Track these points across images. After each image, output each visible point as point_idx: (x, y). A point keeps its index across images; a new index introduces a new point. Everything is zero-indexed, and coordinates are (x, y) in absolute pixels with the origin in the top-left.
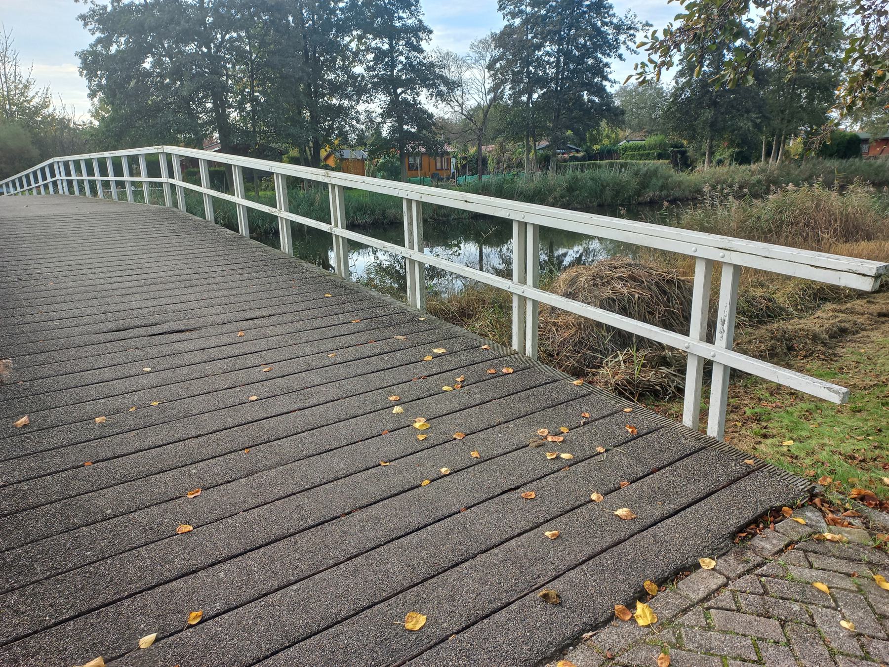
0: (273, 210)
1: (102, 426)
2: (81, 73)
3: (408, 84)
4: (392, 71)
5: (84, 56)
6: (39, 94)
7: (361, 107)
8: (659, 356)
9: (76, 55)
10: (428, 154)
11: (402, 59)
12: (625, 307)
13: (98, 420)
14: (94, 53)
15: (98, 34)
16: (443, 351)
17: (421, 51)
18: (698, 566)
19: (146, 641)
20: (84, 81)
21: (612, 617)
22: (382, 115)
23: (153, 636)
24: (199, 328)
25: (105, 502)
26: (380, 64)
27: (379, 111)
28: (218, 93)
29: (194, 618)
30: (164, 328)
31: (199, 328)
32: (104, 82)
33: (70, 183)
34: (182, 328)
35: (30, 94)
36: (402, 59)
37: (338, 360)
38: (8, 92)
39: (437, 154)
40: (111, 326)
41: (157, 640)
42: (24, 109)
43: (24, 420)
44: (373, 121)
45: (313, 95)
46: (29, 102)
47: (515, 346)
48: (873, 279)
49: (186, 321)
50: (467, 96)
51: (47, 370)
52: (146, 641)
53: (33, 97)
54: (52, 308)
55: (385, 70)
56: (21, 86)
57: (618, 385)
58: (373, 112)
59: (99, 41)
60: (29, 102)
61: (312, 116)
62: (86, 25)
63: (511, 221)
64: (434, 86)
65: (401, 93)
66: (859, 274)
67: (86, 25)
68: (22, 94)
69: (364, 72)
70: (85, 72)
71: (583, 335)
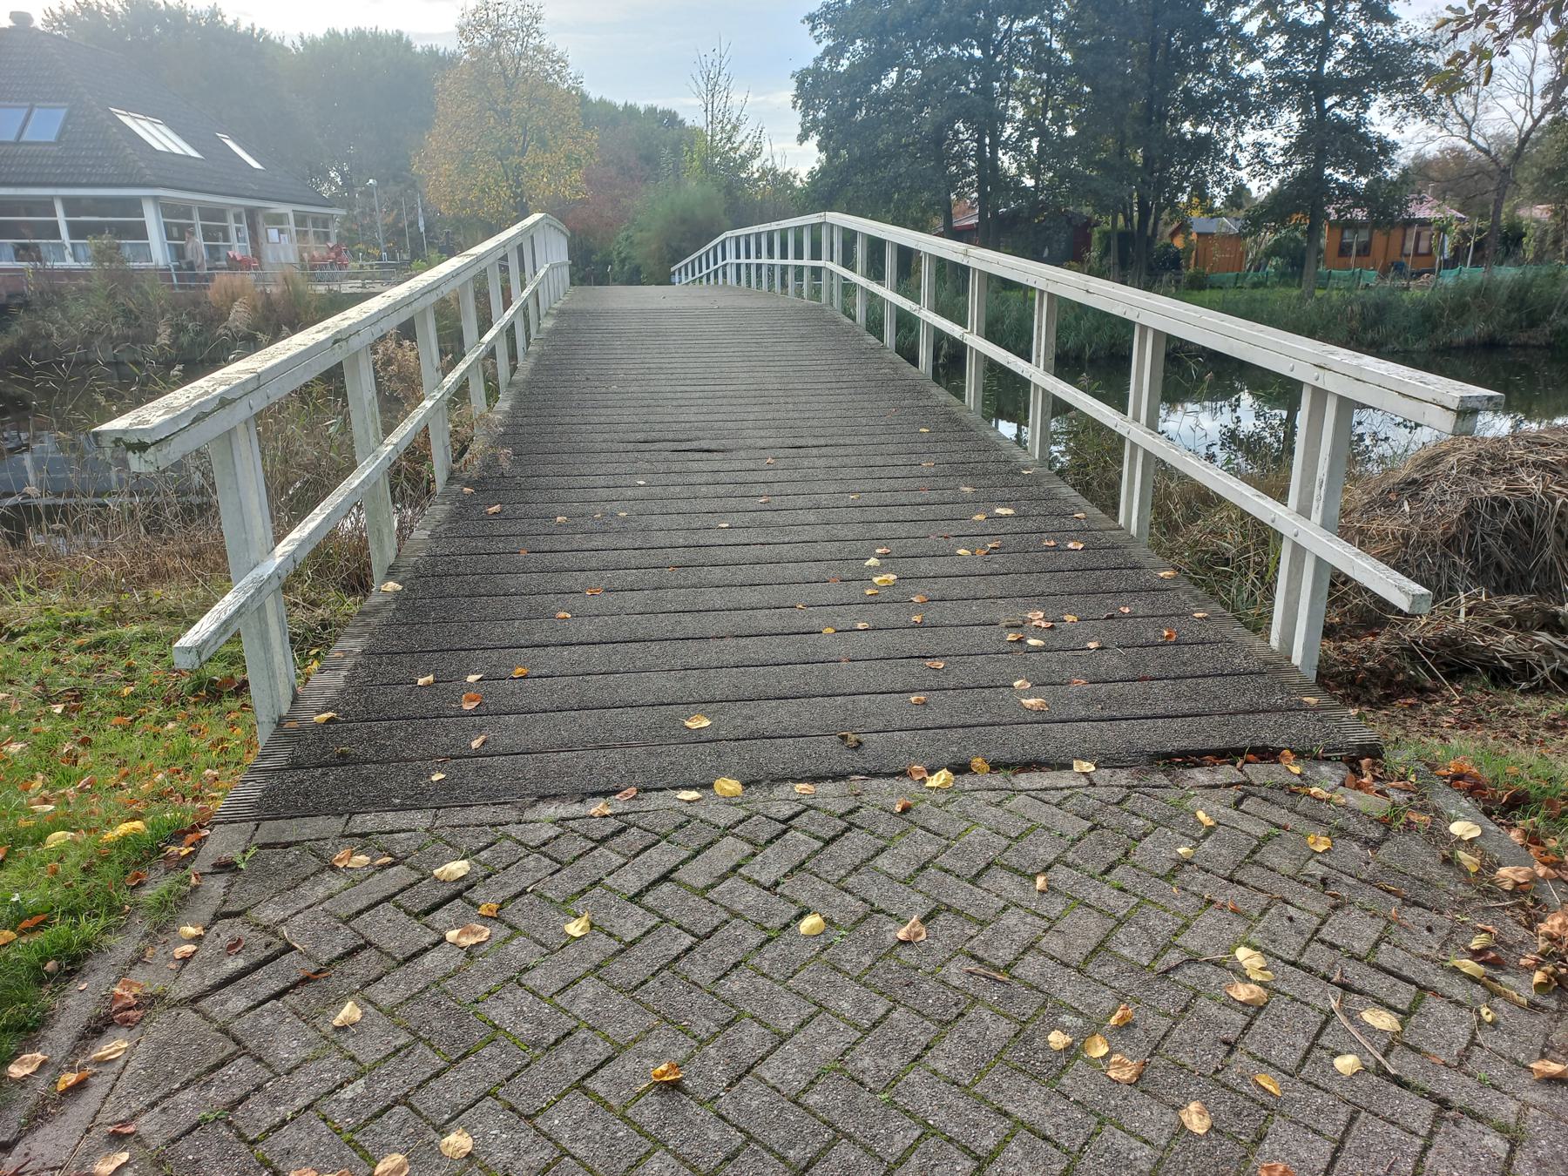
0: (915, 307)
1: (560, 525)
2: (795, 103)
3: (1354, 88)
4: (1320, 66)
5: (801, 78)
6: (750, 138)
7: (1249, 136)
8: (1544, 612)
9: (793, 76)
10: (1373, 224)
11: (1347, 38)
12: (1530, 518)
13: (559, 519)
14: (816, 72)
15: (829, 42)
16: (1010, 512)
17: (1390, 19)
18: (1070, 767)
19: (472, 678)
20: (797, 116)
21: (904, 774)
22: (1285, 151)
23: (479, 677)
24: (731, 450)
25: (512, 583)
26: (1297, 53)
27: (1281, 142)
28: (988, 121)
29: (519, 671)
30: (695, 445)
31: (731, 450)
32: (821, 115)
33: (738, 266)
34: (713, 447)
35: (738, 139)
36: (1347, 38)
37: (859, 503)
38: (712, 136)
39: (1392, 224)
40: (641, 436)
41: (480, 680)
42: (729, 160)
43: (496, 508)
44: (1268, 163)
45: (1155, 115)
46: (736, 150)
47: (1122, 521)
48: (1452, 417)
49: (723, 442)
50: (1489, 103)
51: (548, 469)
52: (472, 678)
53: (743, 142)
54: (597, 412)
55: (1306, 63)
56: (729, 127)
57: (1417, 644)
58: (1269, 145)
59: (828, 51)
60: (736, 150)
61: (1145, 158)
62: (813, 29)
63: (1134, 323)
64: (1410, 86)
65: (1331, 107)
66: (1443, 407)
67: (813, 29)
68: (729, 139)
69: (1262, 71)
70: (800, 101)
71: (1408, 557)
